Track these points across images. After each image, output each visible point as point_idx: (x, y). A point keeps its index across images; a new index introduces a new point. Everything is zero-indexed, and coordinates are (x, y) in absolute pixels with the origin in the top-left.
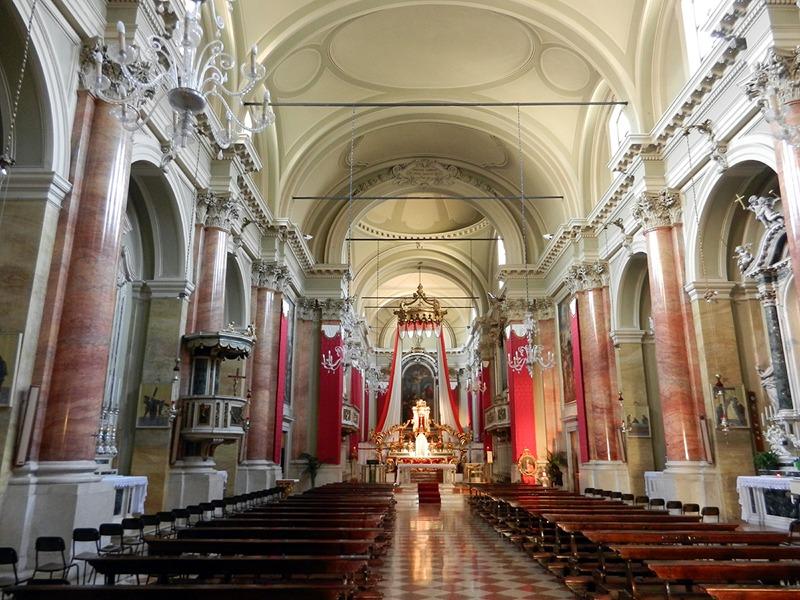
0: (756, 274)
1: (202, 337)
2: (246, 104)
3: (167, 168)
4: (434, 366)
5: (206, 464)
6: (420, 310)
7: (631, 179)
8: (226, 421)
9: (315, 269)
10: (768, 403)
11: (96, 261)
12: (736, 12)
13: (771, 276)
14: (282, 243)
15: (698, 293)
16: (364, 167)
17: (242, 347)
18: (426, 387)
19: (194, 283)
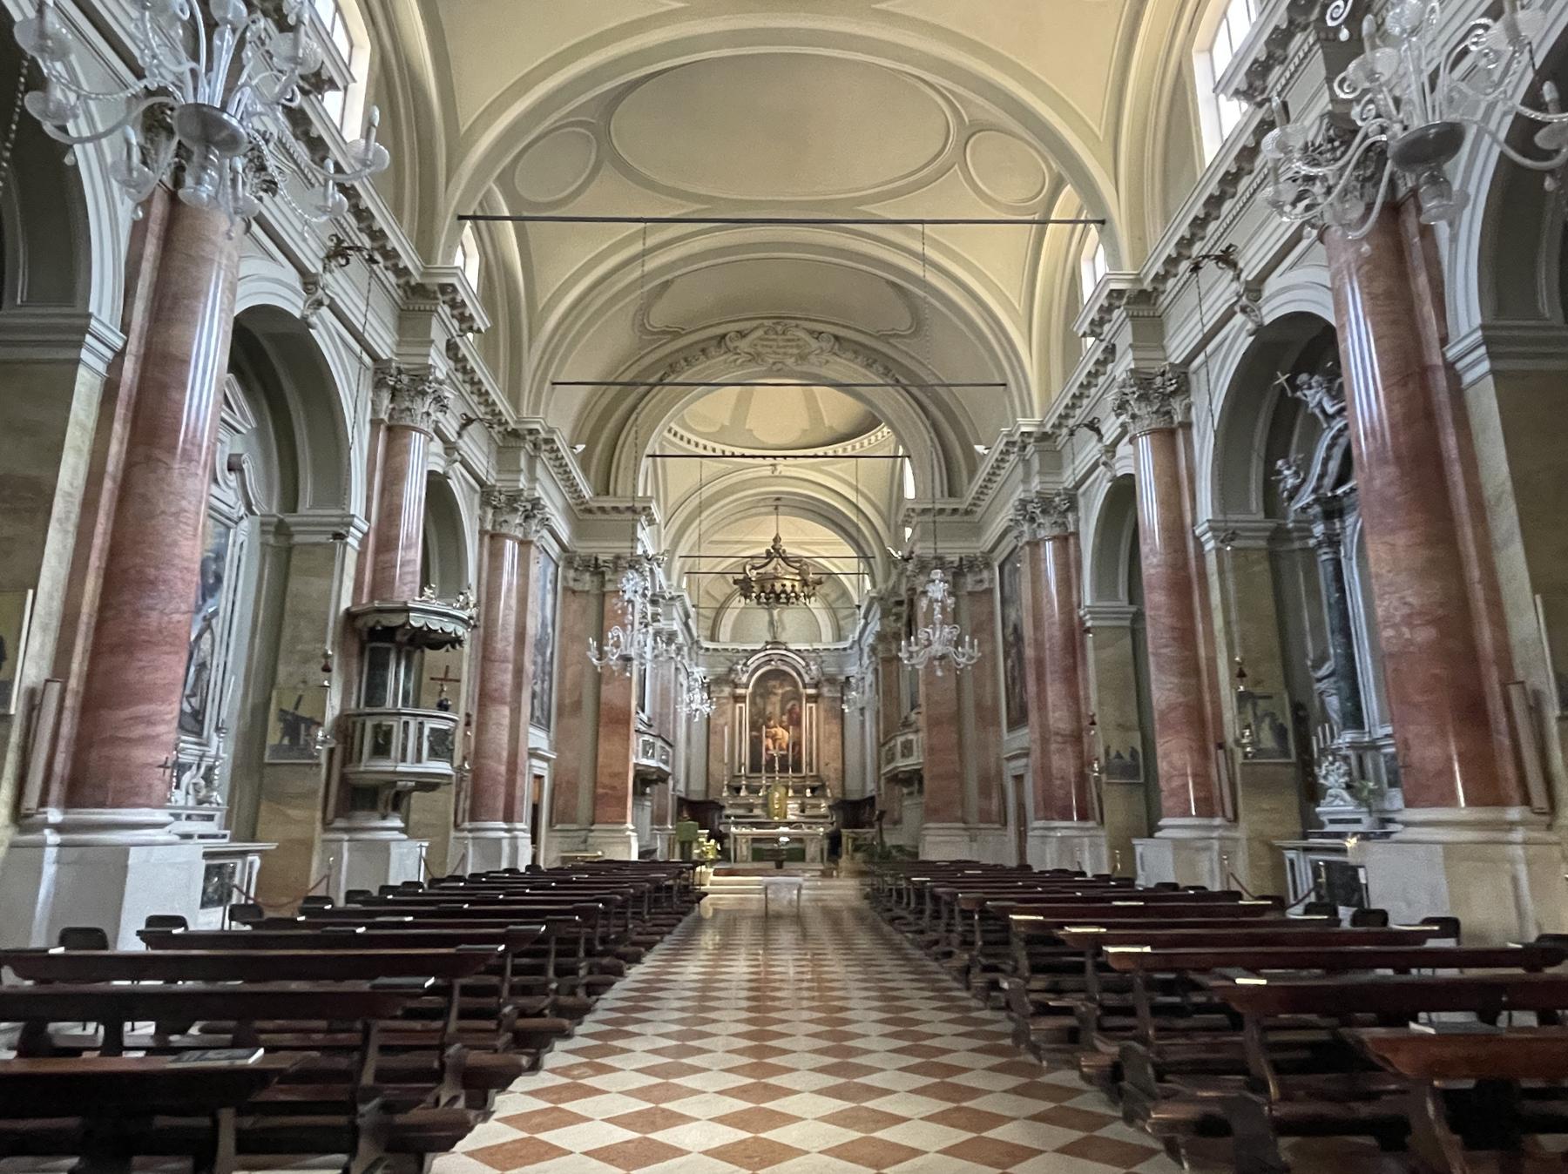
0: (1309, 506)
1: (380, 611)
2: (461, 218)
3: (314, 320)
4: (803, 671)
5: (388, 824)
6: (777, 578)
7: (1111, 351)
8: (419, 751)
9: (594, 505)
10: (1326, 718)
11: (169, 468)
12: (1270, 56)
13: (1333, 510)
14: (532, 459)
15: (1215, 537)
16: (676, 335)
17: (449, 627)
18: (789, 706)
19: (368, 518)
